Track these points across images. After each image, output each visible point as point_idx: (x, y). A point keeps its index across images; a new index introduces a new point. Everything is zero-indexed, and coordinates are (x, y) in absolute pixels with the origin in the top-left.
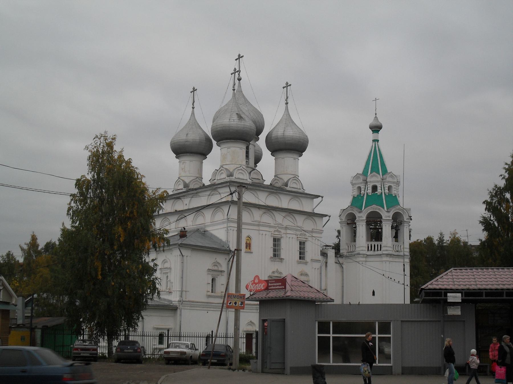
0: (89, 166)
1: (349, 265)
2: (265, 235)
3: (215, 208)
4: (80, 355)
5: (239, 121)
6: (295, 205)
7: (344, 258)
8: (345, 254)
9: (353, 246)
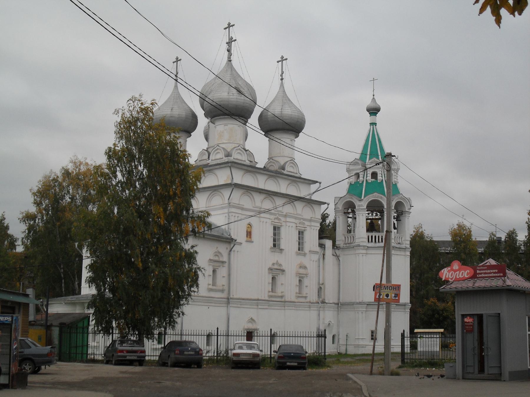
0: (116, 134)
1: (347, 258)
2: (266, 222)
3: (211, 192)
4: (126, 359)
5: (238, 95)
6: (293, 191)
7: (341, 250)
8: (342, 246)
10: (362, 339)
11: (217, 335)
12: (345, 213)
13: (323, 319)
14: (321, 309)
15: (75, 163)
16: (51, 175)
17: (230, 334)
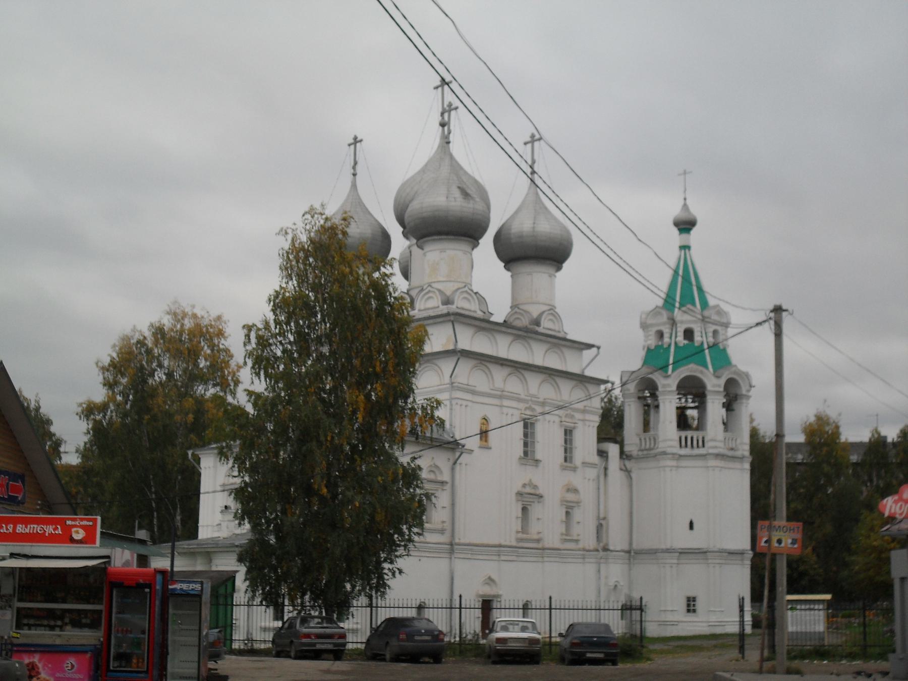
1: (644, 474)
4: (314, 648)
6: (553, 361)
7: (633, 461)
9: (645, 439)
10: (672, 611)
11: (460, 608)
12: (639, 398)
13: (607, 578)
14: (602, 561)
15: (175, 314)
16: (135, 335)
17: (379, 605)
